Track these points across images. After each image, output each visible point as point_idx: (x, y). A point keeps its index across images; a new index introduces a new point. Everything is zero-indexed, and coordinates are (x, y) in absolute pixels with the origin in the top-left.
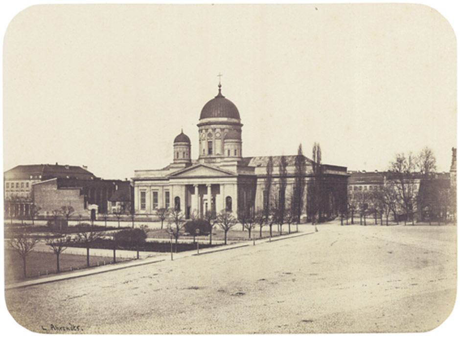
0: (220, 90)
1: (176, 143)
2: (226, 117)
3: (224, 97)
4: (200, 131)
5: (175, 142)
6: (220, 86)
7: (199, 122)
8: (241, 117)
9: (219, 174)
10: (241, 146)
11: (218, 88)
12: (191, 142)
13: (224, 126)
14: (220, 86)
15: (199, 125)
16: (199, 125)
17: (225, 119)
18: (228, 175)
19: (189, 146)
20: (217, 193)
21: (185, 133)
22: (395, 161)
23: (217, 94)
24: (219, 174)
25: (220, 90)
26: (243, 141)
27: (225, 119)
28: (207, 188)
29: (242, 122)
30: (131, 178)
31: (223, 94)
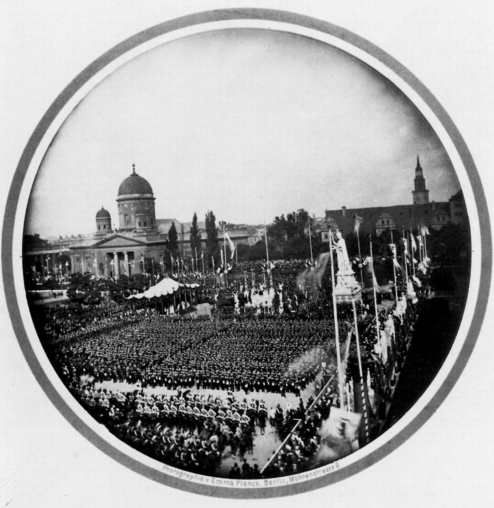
0: (134, 169)
1: (98, 218)
2: (138, 193)
3: (138, 175)
4: (119, 205)
5: (97, 216)
6: (134, 166)
7: (117, 198)
8: (153, 192)
9: (133, 243)
10: (110, 221)
11: (133, 167)
12: (111, 215)
13: (130, 202)
14: (134, 166)
15: (117, 201)
16: (117, 201)
17: (137, 195)
18: (139, 244)
19: (109, 220)
20: (39, 237)
21: (105, 208)
22: (275, 219)
23: (131, 172)
24: (133, 243)
25: (134, 169)
26: (111, 217)
27: (137, 195)
28: (124, 255)
29: (154, 196)
30: (327, 430)
31: (137, 172)
